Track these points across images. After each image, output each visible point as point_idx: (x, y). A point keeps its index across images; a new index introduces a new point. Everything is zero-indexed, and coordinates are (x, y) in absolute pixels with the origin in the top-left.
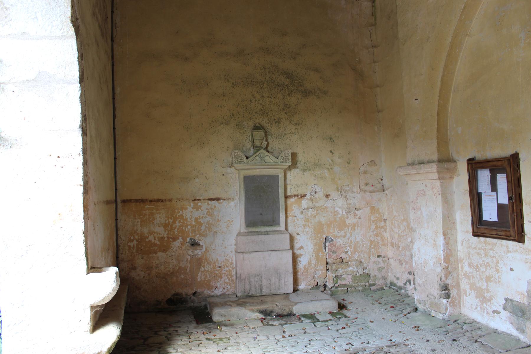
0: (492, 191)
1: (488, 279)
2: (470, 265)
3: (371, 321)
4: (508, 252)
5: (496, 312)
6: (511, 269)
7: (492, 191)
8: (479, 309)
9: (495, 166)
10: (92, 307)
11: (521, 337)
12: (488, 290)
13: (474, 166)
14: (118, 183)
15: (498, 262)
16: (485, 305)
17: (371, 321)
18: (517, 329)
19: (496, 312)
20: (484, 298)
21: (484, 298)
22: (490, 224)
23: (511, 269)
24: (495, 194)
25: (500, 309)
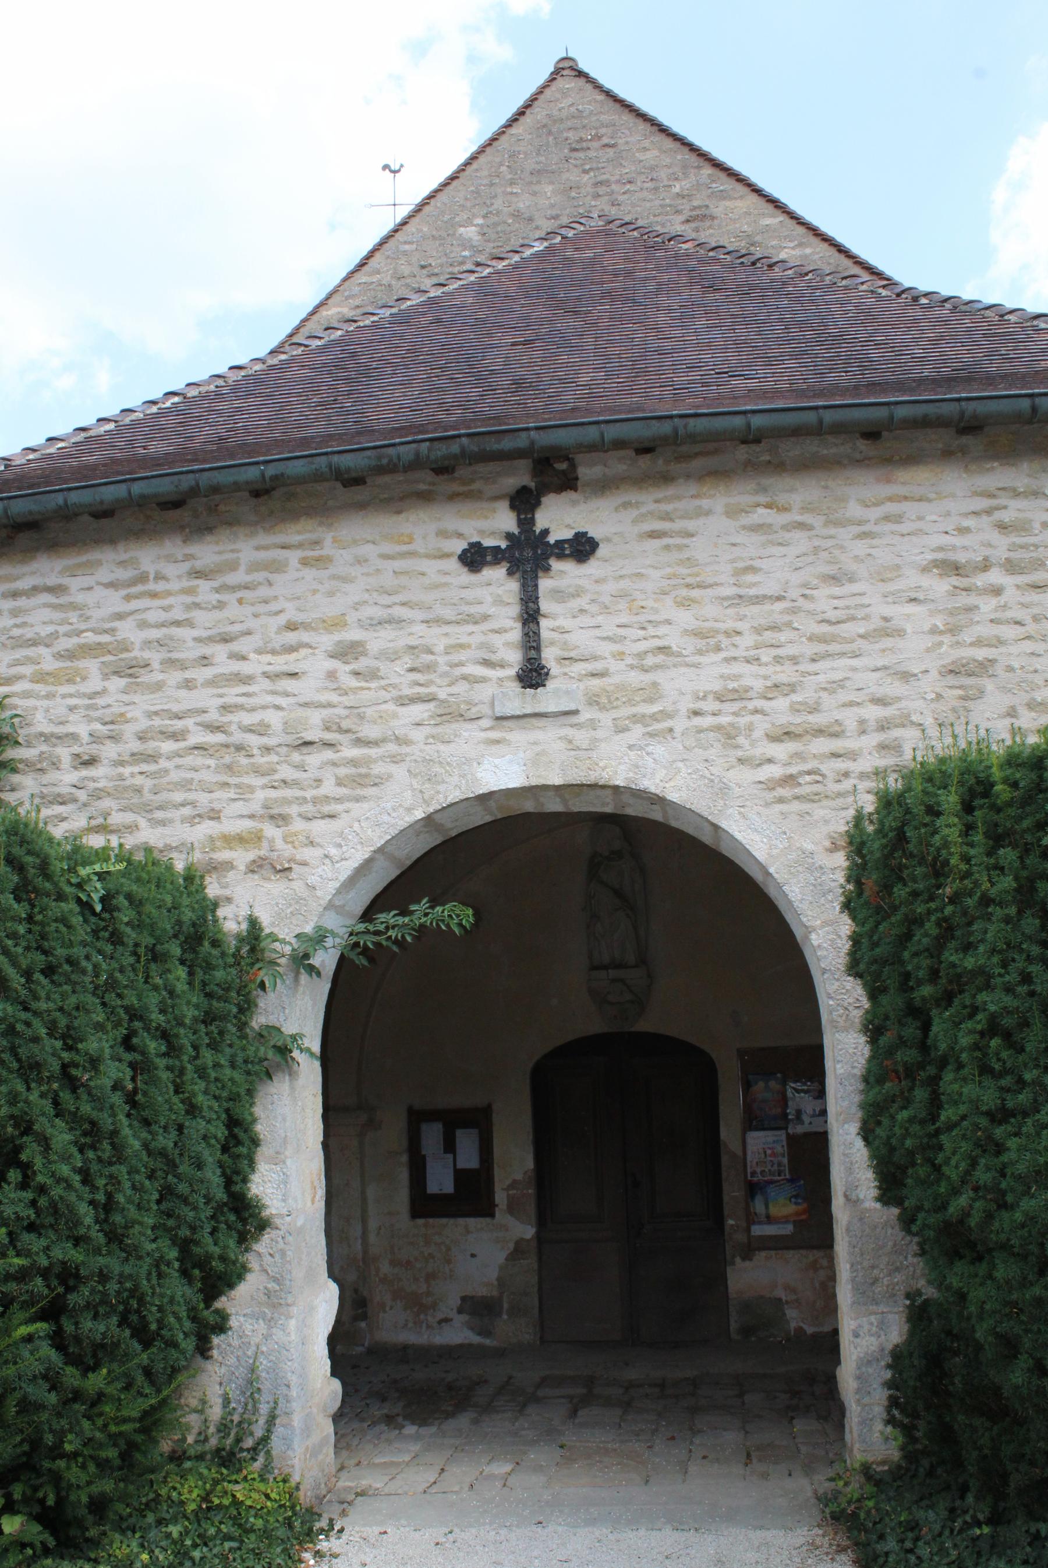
0: (445, 1152)
1: (431, 1277)
2: (393, 1263)
3: (385, 1532)
4: (468, 1232)
5: (447, 1320)
6: (473, 1256)
7: (445, 1152)
8: (410, 1325)
9: (454, 1121)
10: (570, 111)
11: (487, 1342)
12: (428, 1294)
13: (417, 1118)
14: (618, 425)
15: (449, 1249)
16: (422, 1317)
17: (385, 1532)
18: (479, 1334)
19: (447, 1320)
20: (419, 1306)
21: (419, 1306)
22: (441, 1198)
23: (473, 1256)
24: (450, 1156)
25: (453, 1314)
